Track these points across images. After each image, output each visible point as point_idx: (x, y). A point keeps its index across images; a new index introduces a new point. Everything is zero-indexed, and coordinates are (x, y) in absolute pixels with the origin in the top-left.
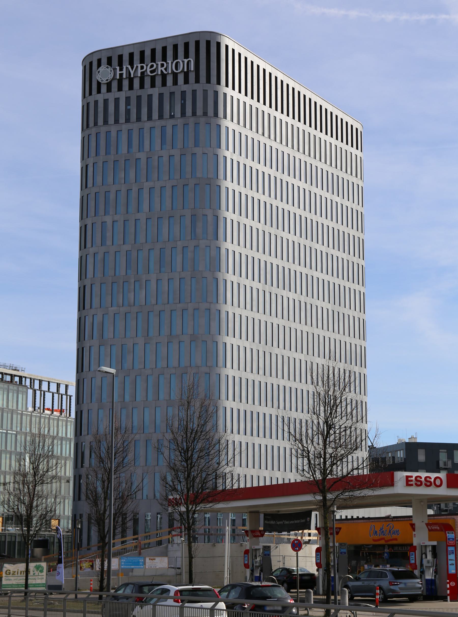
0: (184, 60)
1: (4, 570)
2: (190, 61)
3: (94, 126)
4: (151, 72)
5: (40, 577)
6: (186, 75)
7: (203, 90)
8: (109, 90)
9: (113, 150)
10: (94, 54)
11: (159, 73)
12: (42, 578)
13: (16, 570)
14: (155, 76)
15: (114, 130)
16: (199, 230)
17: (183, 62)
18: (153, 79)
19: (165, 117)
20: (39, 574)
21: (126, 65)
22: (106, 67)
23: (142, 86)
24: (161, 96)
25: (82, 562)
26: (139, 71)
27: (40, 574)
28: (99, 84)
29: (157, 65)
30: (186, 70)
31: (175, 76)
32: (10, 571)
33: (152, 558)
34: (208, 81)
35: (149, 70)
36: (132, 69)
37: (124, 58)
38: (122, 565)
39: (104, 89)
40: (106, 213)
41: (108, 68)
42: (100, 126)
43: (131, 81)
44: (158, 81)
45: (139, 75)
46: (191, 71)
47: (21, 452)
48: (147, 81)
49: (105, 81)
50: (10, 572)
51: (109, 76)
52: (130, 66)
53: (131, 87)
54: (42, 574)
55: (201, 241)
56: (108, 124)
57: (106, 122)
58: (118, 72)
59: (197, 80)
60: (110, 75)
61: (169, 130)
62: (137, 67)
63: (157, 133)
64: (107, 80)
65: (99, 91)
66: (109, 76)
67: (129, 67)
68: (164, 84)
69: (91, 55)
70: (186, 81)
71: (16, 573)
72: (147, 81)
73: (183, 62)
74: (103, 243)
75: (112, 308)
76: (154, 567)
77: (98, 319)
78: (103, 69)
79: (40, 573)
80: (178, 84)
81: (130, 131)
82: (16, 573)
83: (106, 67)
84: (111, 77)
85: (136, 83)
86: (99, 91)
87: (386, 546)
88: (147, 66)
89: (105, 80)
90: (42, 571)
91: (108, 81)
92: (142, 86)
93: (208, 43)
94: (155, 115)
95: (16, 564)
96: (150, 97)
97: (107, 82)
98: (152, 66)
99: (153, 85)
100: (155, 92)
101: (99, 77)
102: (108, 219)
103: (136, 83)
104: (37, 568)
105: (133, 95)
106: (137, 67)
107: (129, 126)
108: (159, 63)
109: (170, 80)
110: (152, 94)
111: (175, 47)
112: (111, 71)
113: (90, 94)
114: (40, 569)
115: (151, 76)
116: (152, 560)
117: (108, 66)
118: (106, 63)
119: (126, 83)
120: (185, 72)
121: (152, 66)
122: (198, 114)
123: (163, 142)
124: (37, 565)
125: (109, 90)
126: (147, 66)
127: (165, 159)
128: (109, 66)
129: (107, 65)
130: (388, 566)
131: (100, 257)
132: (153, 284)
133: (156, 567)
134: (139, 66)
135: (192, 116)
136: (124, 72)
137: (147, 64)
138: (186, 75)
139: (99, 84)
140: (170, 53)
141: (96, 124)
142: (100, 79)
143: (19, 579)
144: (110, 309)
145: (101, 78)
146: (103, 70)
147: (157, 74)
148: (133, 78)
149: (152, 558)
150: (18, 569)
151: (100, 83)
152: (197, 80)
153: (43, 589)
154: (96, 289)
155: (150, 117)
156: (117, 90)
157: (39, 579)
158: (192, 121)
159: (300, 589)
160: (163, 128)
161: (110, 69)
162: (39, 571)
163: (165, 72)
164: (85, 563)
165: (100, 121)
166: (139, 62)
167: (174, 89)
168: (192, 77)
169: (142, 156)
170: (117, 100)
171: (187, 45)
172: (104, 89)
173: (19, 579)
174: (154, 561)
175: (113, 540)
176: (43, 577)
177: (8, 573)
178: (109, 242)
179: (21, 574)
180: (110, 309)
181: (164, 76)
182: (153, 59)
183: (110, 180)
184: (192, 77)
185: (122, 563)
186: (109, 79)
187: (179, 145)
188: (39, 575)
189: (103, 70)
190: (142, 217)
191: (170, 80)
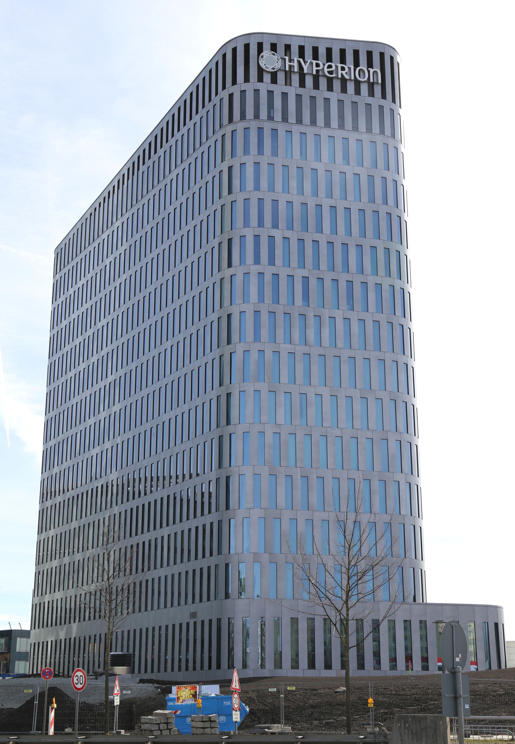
8: (274, 80)
15: (282, 128)
17: (369, 71)
18: (330, 81)
26: (315, 69)
28: (261, 71)
29: (337, 67)
35: (326, 70)
36: (305, 62)
39: (267, 78)
42: (263, 121)
44: (337, 85)
46: (294, 72)
47: (310, 555)
49: (270, 69)
61: (353, 145)
64: (273, 69)
67: (301, 60)
69: (249, 35)
73: (369, 71)
74: (272, 261)
78: (268, 55)
84: (278, 65)
86: (260, 79)
87: (396, 664)
91: (275, 70)
93: (382, 55)
98: (330, 67)
100: (249, 88)
103: (309, 81)
115: (328, 77)
120: (286, 72)
122: (290, 120)
125: (274, 80)
126: (324, 65)
136: (296, 64)
139: (261, 71)
144: (281, 345)
146: (267, 55)
159: (485, 734)
163: (347, 77)
166: (312, 59)
168: (378, 90)
169: (321, 168)
172: (267, 78)
178: (279, 262)
184: (378, 90)
189: (267, 55)
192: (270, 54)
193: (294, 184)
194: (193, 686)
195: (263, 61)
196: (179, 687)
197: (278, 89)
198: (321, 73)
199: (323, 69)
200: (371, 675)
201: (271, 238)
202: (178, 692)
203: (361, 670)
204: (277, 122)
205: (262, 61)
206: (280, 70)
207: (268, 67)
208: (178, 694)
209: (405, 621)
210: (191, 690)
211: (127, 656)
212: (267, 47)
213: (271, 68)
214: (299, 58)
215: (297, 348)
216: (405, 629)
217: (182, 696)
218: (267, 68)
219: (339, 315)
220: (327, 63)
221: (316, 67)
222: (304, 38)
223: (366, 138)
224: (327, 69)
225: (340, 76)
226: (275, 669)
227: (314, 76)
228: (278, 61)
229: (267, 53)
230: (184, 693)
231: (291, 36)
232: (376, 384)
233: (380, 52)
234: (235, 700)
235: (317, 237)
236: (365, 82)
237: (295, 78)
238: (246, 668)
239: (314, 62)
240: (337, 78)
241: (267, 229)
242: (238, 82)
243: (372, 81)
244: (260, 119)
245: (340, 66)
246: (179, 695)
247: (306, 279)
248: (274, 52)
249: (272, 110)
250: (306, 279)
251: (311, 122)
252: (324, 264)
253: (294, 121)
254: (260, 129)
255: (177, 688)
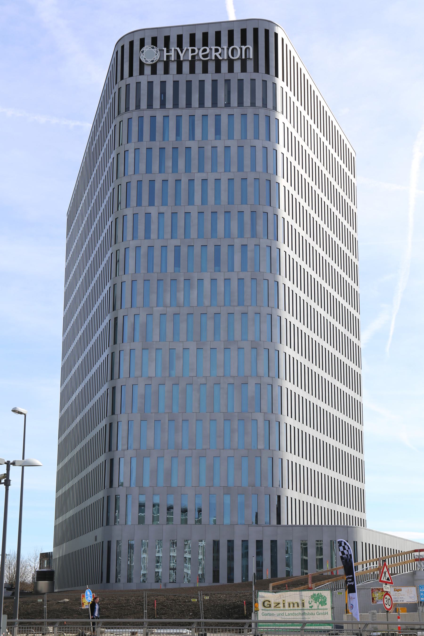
0: (242, 46)
1: (260, 601)
2: (249, 48)
3: (126, 111)
4: (204, 56)
5: (320, 611)
6: (244, 63)
7: (262, 80)
8: (154, 71)
9: (159, 136)
10: (135, 33)
11: (213, 58)
12: (327, 613)
13: (281, 601)
14: (208, 60)
16: (260, 228)
17: (241, 49)
18: (205, 65)
19: (219, 105)
20: (318, 607)
21: (173, 47)
22: (151, 47)
23: (192, 70)
24: (215, 82)
25: (374, 591)
26: (190, 55)
27: (320, 607)
28: (142, 65)
29: (211, 49)
30: (243, 57)
31: (231, 62)
32: (269, 601)
33: (398, 588)
34: (267, 71)
35: (201, 54)
37: (171, 40)
38: (422, 597)
39: (148, 70)
40: (151, 203)
41: (153, 48)
42: (144, 110)
43: (180, 64)
44: (212, 66)
45: (190, 59)
46: (249, 59)
48: (199, 66)
49: (150, 62)
50: (270, 603)
51: (155, 57)
52: (180, 48)
53: (180, 71)
54: (324, 607)
55: (261, 240)
56: (152, 108)
57: (150, 106)
58: (165, 54)
59: (256, 70)
60: (155, 56)
61: (224, 120)
62: (187, 50)
63: (211, 122)
64: (152, 61)
65: (142, 72)
66: (155, 57)
67: (178, 49)
68: (218, 70)
70: (244, 69)
71: (281, 605)
72: (199, 66)
73: (241, 49)
74: (147, 236)
75: (158, 308)
76: (400, 601)
77: (142, 318)
78: (148, 49)
79: (320, 605)
80: (235, 72)
81: (179, 117)
82: (281, 605)
83: (151, 47)
84: (156, 58)
85: (186, 67)
86: (142, 72)
88: (199, 49)
89: (149, 61)
90: (323, 603)
91: (154, 62)
92: (192, 70)
94: (208, 102)
95: (279, 592)
96: (202, 83)
97: (152, 63)
98: (205, 50)
99: (205, 70)
100: (208, 78)
101: (142, 57)
102: (153, 211)
103: (186, 67)
104: (315, 598)
105: (182, 79)
106: (187, 50)
107: (178, 112)
108: (214, 48)
109: (224, 66)
110: (204, 80)
111: (231, 33)
112: (157, 52)
113: (122, 78)
114: (320, 600)
115: (203, 61)
116: (397, 590)
117: (153, 46)
118: (151, 43)
119: (173, 67)
120: (242, 60)
121: (205, 50)
122: (257, 105)
123: (218, 132)
124: (314, 595)
125: (154, 71)
126: (199, 49)
127: (221, 150)
128: (154, 46)
129: (152, 45)
130: (44, 615)
131: (144, 250)
132: (207, 284)
133: (403, 601)
134: (190, 49)
135: (251, 106)
136: (172, 53)
137: (199, 48)
138: (244, 63)
139: (142, 65)
140: (224, 39)
141: (138, 107)
142: (144, 60)
143: (287, 614)
144: (155, 309)
145: (145, 59)
146: (147, 50)
147: (211, 60)
148: (182, 61)
149: (398, 588)
150: (284, 599)
151: (144, 63)
152: (256, 70)
153: (330, 628)
154: (140, 285)
155: (202, 104)
156: (163, 72)
157: (319, 614)
158: (250, 112)
160: (218, 117)
161: (155, 49)
162: (318, 603)
163: (220, 58)
164: (377, 593)
165: (144, 104)
166: (189, 45)
167: (229, 76)
168: (250, 65)
169: (194, 145)
170: (163, 84)
171: (244, 32)
172: (148, 70)
173: (287, 614)
174: (400, 592)
175: (354, 563)
176: (326, 611)
177: (267, 604)
178: (154, 235)
179: (289, 607)
180: (155, 309)
181: (218, 62)
182: (205, 43)
183: (155, 167)
184: (250, 65)
185: (422, 594)
186: (155, 60)
187: (237, 134)
188: (318, 609)
189: (147, 50)
190: (194, 210)
191: (224, 66)
192: (150, 48)
193: (169, 163)
194: (380, 588)
195: (143, 55)
196: (373, 589)
197: (157, 79)
198: (196, 58)
199: (198, 54)
200: (153, 588)
201: (148, 215)
202: (373, 594)
203: (216, 583)
204: (156, 109)
205: (143, 55)
206: (159, 61)
207: (148, 60)
208: (373, 595)
209: (229, 541)
210: (383, 592)
211: (47, 572)
212: (148, 41)
213: (151, 61)
214: (177, 47)
215: (168, 309)
216: (257, 548)
217: (376, 597)
218: (147, 61)
219: (207, 277)
220: (203, 47)
221: (166, 53)
222: (182, 27)
223: (237, 112)
224: (191, 53)
225: (213, 58)
226: (107, 583)
227: (165, 62)
228: (157, 53)
229: (147, 48)
230: (378, 595)
231: (170, 27)
232: (237, 335)
233: (265, 29)
234: (387, 601)
235: (189, 209)
236: (238, 59)
237: (173, 67)
238: (130, 582)
239: (190, 49)
240: (211, 60)
241: (144, 207)
242: (124, 77)
243: (243, 57)
244: (244, 106)
245: (214, 48)
246: (373, 596)
247: (177, 248)
248: (153, 46)
249: (162, 99)
250: (177, 248)
251: (239, 103)
252: (194, 233)
253: (210, 105)
254: (192, 117)
255: (371, 590)
